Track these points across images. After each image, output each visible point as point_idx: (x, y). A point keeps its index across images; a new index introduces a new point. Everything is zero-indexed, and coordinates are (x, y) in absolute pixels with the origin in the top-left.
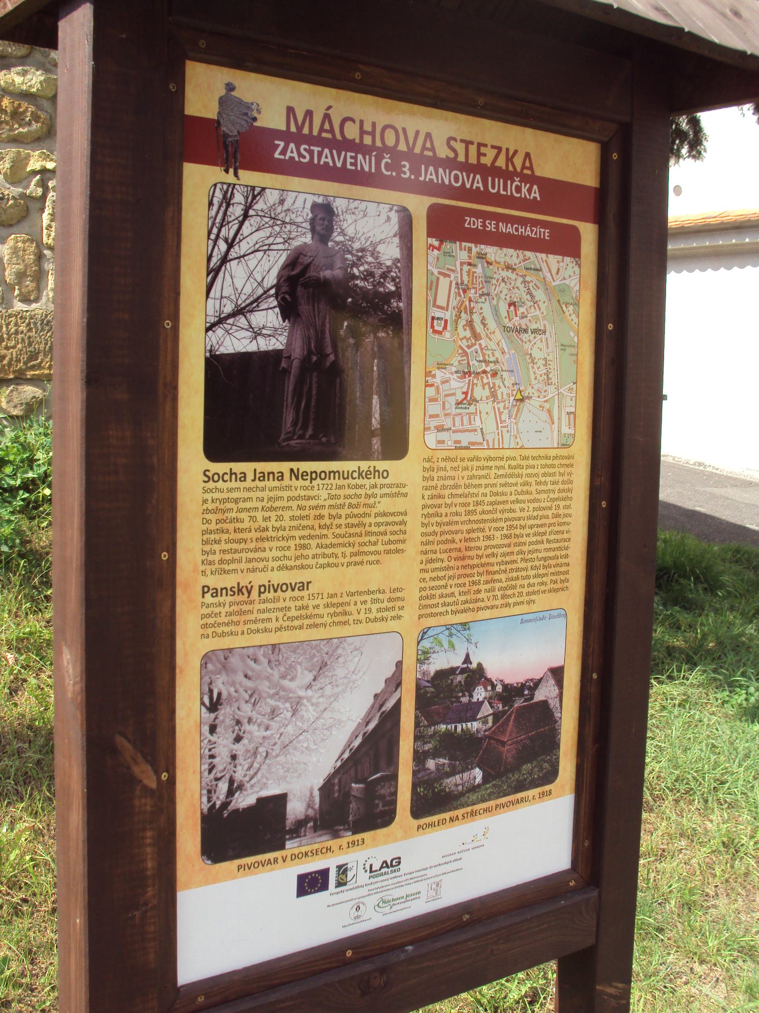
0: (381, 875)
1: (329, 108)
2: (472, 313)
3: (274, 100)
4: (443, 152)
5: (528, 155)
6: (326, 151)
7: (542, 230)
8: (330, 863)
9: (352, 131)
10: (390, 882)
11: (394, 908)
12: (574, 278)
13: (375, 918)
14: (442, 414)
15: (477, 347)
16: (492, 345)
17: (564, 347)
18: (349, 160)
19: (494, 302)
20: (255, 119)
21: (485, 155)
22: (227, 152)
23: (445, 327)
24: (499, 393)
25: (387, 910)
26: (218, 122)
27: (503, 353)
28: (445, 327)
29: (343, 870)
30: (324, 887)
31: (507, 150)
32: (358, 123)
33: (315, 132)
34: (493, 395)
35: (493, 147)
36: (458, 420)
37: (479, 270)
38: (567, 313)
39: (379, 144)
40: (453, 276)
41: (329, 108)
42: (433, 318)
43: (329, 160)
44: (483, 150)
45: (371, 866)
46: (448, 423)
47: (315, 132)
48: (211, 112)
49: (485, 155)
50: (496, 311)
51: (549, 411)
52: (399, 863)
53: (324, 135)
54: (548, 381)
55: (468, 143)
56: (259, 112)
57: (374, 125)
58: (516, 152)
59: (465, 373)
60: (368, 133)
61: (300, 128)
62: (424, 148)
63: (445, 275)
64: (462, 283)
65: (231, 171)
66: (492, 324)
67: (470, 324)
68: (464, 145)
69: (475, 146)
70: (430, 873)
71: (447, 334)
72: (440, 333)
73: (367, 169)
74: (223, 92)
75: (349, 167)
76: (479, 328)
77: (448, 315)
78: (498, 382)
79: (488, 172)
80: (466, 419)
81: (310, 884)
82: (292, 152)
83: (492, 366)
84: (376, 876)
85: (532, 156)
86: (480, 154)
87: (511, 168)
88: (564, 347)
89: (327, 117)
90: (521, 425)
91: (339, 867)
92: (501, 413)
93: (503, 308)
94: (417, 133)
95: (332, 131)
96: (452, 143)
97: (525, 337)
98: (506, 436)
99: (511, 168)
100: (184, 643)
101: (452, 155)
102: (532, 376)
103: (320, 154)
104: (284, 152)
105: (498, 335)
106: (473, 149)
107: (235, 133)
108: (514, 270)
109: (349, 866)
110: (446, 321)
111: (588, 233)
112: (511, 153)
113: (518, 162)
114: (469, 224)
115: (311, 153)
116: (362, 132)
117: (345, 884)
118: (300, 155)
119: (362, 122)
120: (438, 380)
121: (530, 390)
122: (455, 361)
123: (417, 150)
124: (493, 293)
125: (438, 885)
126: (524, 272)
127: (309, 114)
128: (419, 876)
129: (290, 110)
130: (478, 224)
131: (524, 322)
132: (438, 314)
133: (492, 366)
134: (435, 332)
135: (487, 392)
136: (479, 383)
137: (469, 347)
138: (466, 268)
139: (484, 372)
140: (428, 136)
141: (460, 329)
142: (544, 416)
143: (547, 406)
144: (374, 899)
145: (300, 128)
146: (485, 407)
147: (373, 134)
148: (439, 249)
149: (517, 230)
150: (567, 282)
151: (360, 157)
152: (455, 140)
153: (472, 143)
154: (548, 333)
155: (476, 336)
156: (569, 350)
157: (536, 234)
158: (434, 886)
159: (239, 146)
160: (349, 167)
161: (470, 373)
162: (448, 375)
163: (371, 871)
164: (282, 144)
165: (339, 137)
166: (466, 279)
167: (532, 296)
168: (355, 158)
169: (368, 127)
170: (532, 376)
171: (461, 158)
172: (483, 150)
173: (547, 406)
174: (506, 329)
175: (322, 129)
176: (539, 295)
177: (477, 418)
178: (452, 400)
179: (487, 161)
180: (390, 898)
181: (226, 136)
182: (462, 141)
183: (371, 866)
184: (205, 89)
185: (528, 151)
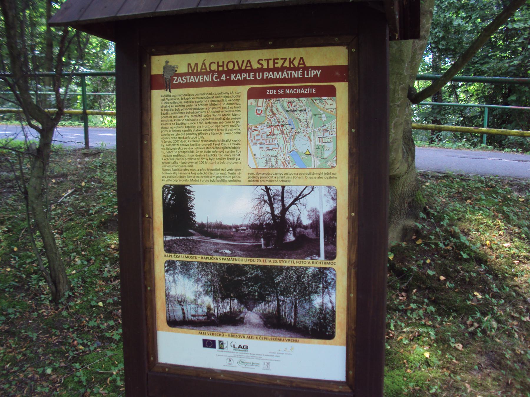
1: (205, 60)
2: (272, 107)
3: (181, 62)
4: (256, 66)
5: (302, 59)
6: (192, 77)
8: (217, 339)
9: (214, 67)
11: (247, 366)
12: (338, 106)
13: (237, 367)
14: (261, 139)
16: (281, 117)
17: (315, 115)
18: (201, 79)
20: (176, 71)
21: (277, 63)
23: (262, 112)
24: (285, 132)
25: (244, 366)
26: (163, 75)
27: (286, 118)
28: (262, 112)
30: (214, 346)
31: (290, 59)
32: (216, 63)
33: (199, 70)
34: (283, 133)
35: (281, 59)
36: (268, 141)
41: (205, 60)
43: (193, 80)
44: (276, 61)
46: (264, 142)
47: (199, 70)
48: (161, 72)
49: (277, 63)
50: (282, 106)
51: (309, 137)
52: (247, 348)
53: (202, 71)
54: (308, 126)
55: (268, 60)
56: (177, 68)
57: (223, 62)
58: (294, 58)
59: (270, 126)
60: (221, 66)
61: (193, 70)
62: (246, 66)
65: (168, 90)
66: (281, 109)
67: (272, 111)
69: (272, 60)
70: (263, 357)
71: (262, 114)
72: (259, 114)
73: (208, 80)
74: (164, 64)
75: (201, 81)
76: (275, 111)
77: (262, 109)
78: (284, 128)
80: (271, 141)
81: (208, 344)
82: (239, 77)
83: (281, 123)
85: (304, 59)
86: (274, 63)
87: (292, 66)
88: (315, 115)
90: (295, 142)
91: (220, 341)
92: (286, 139)
94: (243, 61)
95: (206, 69)
96: (260, 62)
97: (296, 113)
98: (289, 146)
99: (292, 66)
101: (260, 66)
102: (300, 126)
103: (190, 79)
104: (177, 81)
105: (284, 113)
106: (271, 63)
111: (342, 88)
113: (296, 63)
114: (269, 92)
115: (186, 79)
116: (218, 66)
117: (223, 349)
118: (183, 80)
119: (218, 63)
120: (259, 129)
121: (299, 130)
122: (266, 122)
123: (243, 68)
127: (196, 64)
129: (189, 65)
130: (274, 92)
131: (295, 108)
132: (259, 108)
133: (281, 123)
134: (258, 114)
135: (280, 132)
136: (276, 129)
139: (278, 125)
140: (249, 61)
141: (268, 113)
142: (307, 139)
143: (308, 135)
145: (193, 70)
146: (279, 137)
147: (223, 66)
149: (296, 91)
151: (205, 76)
152: (262, 60)
153: (271, 59)
154: (307, 111)
155: (274, 114)
156: (318, 116)
157: (307, 91)
159: (165, 83)
160: (201, 81)
161: (272, 126)
162: (263, 127)
164: (176, 78)
165: (208, 70)
168: (203, 77)
169: (221, 64)
170: (300, 126)
171: (265, 67)
172: (276, 61)
173: (308, 135)
174: (287, 111)
175: (202, 69)
177: (276, 140)
178: (265, 135)
179: (279, 65)
181: (166, 79)
182: (265, 60)
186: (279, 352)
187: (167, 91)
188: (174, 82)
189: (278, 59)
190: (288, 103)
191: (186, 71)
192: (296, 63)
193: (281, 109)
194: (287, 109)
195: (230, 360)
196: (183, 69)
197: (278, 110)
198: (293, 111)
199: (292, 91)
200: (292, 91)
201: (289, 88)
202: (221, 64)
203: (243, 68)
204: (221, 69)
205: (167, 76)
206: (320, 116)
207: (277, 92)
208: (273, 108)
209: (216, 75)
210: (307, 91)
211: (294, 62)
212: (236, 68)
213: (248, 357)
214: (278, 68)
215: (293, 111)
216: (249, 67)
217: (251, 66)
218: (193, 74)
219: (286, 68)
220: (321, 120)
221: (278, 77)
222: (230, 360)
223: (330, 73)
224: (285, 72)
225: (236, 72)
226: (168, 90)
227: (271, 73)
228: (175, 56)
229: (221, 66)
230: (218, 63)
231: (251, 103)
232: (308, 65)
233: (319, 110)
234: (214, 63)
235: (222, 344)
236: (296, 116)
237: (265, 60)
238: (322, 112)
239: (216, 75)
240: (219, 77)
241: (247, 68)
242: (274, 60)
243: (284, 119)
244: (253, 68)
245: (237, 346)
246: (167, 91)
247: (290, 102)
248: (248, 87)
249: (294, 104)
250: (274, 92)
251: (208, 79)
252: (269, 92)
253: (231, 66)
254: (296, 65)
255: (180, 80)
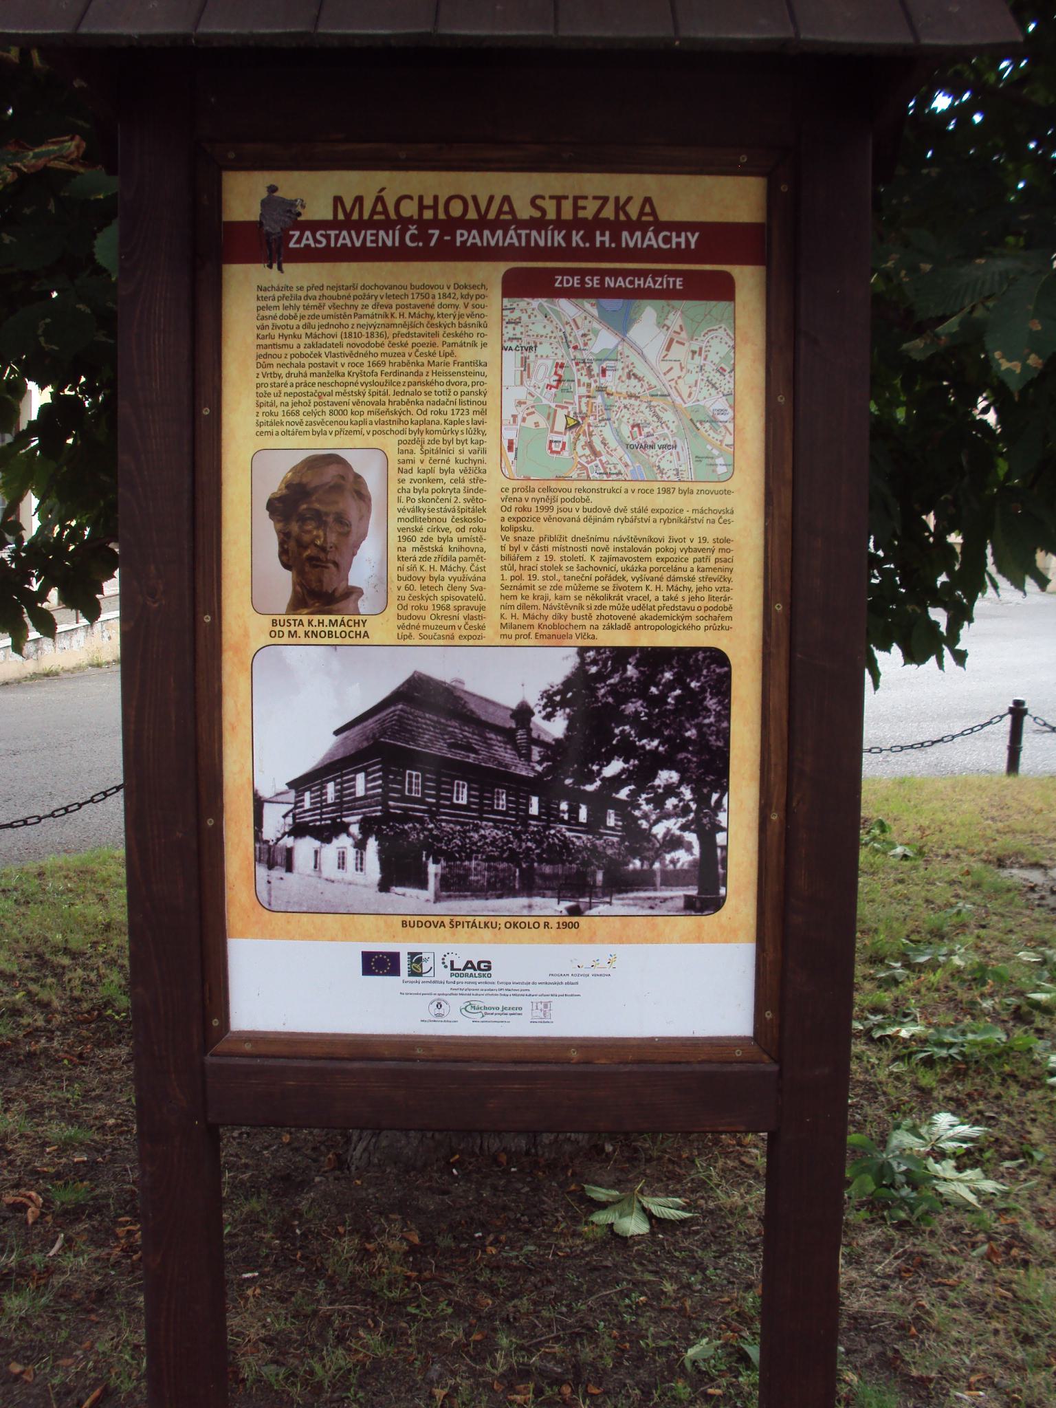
0: (466, 975)
1: (383, 189)
2: (591, 435)
3: (317, 192)
4: (525, 212)
5: (648, 200)
6: (345, 233)
7: (671, 280)
8: (403, 949)
9: (409, 209)
10: (478, 986)
11: (487, 1018)
13: (461, 1024)
15: (597, 462)
16: (614, 460)
17: (698, 459)
18: (369, 238)
19: (616, 425)
20: (299, 214)
21: (584, 208)
22: (271, 250)
23: (563, 448)
26: (261, 223)
27: (626, 465)
28: (563, 448)
29: (416, 958)
30: (395, 971)
31: (617, 199)
33: (366, 216)
35: (595, 198)
37: (599, 400)
38: (702, 430)
39: (442, 216)
40: (570, 407)
41: (383, 189)
42: (551, 442)
44: (581, 203)
45: (452, 962)
47: (366, 216)
49: (584, 208)
50: (617, 433)
52: (489, 968)
53: (376, 217)
55: (559, 199)
56: (303, 206)
57: (436, 198)
58: (629, 199)
60: (428, 207)
61: (348, 215)
62: (500, 212)
63: (563, 407)
64: (581, 412)
65: (275, 266)
66: (613, 443)
67: (590, 445)
68: (554, 202)
69: (570, 201)
70: (533, 989)
71: (565, 454)
72: (558, 453)
73: (389, 243)
75: (369, 244)
79: (590, 227)
81: (379, 964)
84: (459, 975)
86: (576, 208)
87: (622, 217)
88: (698, 459)
89: (380, 199)
91: (412, 955)
93: (626, 430)
94: (491, 198)
95: (385, 212)
97: (650, 452)
99: (622, 217)
100: (235, 702)
101: (538, 214)
103: (337, 237)
104: (299, 241)
105: (620, 451)
106: (567, 206)
107: (279, 230)
108: (637, 398)
109: (424, 956)
110: (564, 444)
111: (748, 281)
112: (622, 202)
113: (633, 211)
114: (561, 282)
115: (328, 237)
116: (422, 207)
117: (420, 974)
118: (316, 241)
119: (421, 198)
123: (492, 215)
124: (614, 418)
125: (546, 1006)
126: (650, 398)
127: (359, 200)
128: (520, 988)
129: (338, 200)
130: (575, 282)
131: (649, 441)
134: (553, 452)
137: (588, 463)
138: (584, 400)
140: (506, 199)
141: (579, 449)
144: (460, 1001)
145: (348, 215)
147: (435, 207)
148: (557, 387)
149: (632, 282)
150: (701, 403)
151: (382, 233)
152: (543, 198)
153: (566, 198)
155: (596, 454)
156: (705, 461)
157: (661, 284)
158: (541, 1006)
159: (271, 243)
160: (369, 244)
163: (452, 969)
164: (297, 234)
165: (393, 216)
166: (584, 409)
167: (658, 417)
168: (377, 235)
169: (428, 201)
171: (551, 215)
172: (581, 203)
175: (374, 212)
176: (668, 416)
180: (481, 1005)
181: (269, 234)
182: (551, 197)
183: (452, 962)
184: (244, 196)
185: (648, 195)
186: (581, 971)
187: (270, 267)
188: (292, 245)
189: (585, 198)
190: (633, 427)
191: (330, 217)
192: (633, 211)
193: (613, 443)
194: (630, 441)
195: (439, 1006)
196: (320, 209)
197: (605, 445)
198: (644, 447)
199: (620, 282)
200: (620, 282)
201: (615, 273)
202: (428, 201)
203: (492, 215)
204: (428, 214)
205: (272, 227)
206: (710, 461)
207: (582, 282)
208: (594, 438)
209: (413, 230)
210: (661, 284)
211: (628, 208)
212: (472, 215)
213: (491, 993)
214: (585, 220)
215: (644, 447)
216: (506, 213)
217: (512, 211)
218: (348, 224)
219: (551, 222)
220: (714, 471)
221: (631, 245)
222: (439, 1006)
223: (721, 241)
224: (650, 234)
225: (469, 225)
226: (275, 266)
227: (474, 232)
228: (296, 175)
229: (428, 207)
230: (421, 198)
231: (537, 424)
232: (664, 217)
233: (709, 447)
234: (411, 198)
235: (419, 961)
236: (653, 460)
237: (551, 197)
238: (716, 452)
239: (413, 230)
240: (423, 236)
241: (502, 217)
242: (576, 199)
243: (620, 467)
244: (519, 217)
245: (459, 964)
246: (270, 267)
247: (638, 425)
248: (503, 267)
249: (646, 430)
250: (575, 282)
251: (389, 239)
252: (561, 282)
253: (456, 209)
254: (634, 217)
255: (308, 239)
